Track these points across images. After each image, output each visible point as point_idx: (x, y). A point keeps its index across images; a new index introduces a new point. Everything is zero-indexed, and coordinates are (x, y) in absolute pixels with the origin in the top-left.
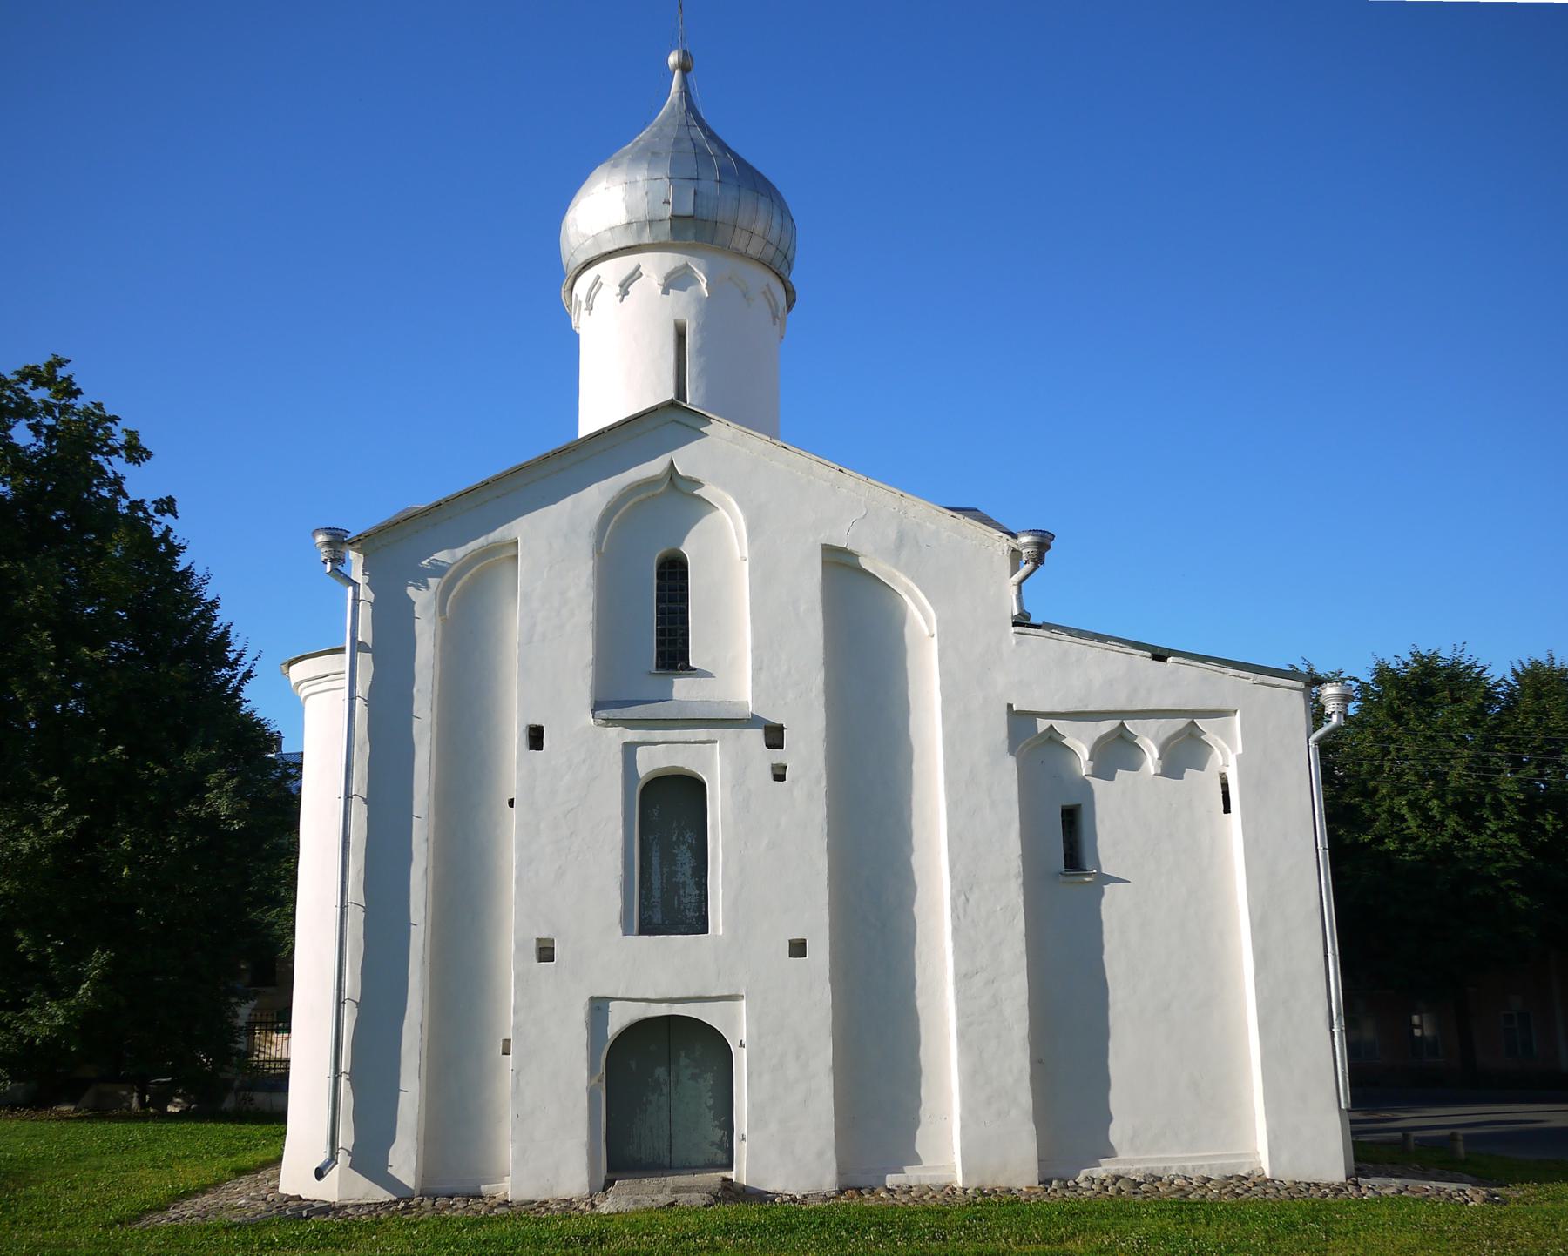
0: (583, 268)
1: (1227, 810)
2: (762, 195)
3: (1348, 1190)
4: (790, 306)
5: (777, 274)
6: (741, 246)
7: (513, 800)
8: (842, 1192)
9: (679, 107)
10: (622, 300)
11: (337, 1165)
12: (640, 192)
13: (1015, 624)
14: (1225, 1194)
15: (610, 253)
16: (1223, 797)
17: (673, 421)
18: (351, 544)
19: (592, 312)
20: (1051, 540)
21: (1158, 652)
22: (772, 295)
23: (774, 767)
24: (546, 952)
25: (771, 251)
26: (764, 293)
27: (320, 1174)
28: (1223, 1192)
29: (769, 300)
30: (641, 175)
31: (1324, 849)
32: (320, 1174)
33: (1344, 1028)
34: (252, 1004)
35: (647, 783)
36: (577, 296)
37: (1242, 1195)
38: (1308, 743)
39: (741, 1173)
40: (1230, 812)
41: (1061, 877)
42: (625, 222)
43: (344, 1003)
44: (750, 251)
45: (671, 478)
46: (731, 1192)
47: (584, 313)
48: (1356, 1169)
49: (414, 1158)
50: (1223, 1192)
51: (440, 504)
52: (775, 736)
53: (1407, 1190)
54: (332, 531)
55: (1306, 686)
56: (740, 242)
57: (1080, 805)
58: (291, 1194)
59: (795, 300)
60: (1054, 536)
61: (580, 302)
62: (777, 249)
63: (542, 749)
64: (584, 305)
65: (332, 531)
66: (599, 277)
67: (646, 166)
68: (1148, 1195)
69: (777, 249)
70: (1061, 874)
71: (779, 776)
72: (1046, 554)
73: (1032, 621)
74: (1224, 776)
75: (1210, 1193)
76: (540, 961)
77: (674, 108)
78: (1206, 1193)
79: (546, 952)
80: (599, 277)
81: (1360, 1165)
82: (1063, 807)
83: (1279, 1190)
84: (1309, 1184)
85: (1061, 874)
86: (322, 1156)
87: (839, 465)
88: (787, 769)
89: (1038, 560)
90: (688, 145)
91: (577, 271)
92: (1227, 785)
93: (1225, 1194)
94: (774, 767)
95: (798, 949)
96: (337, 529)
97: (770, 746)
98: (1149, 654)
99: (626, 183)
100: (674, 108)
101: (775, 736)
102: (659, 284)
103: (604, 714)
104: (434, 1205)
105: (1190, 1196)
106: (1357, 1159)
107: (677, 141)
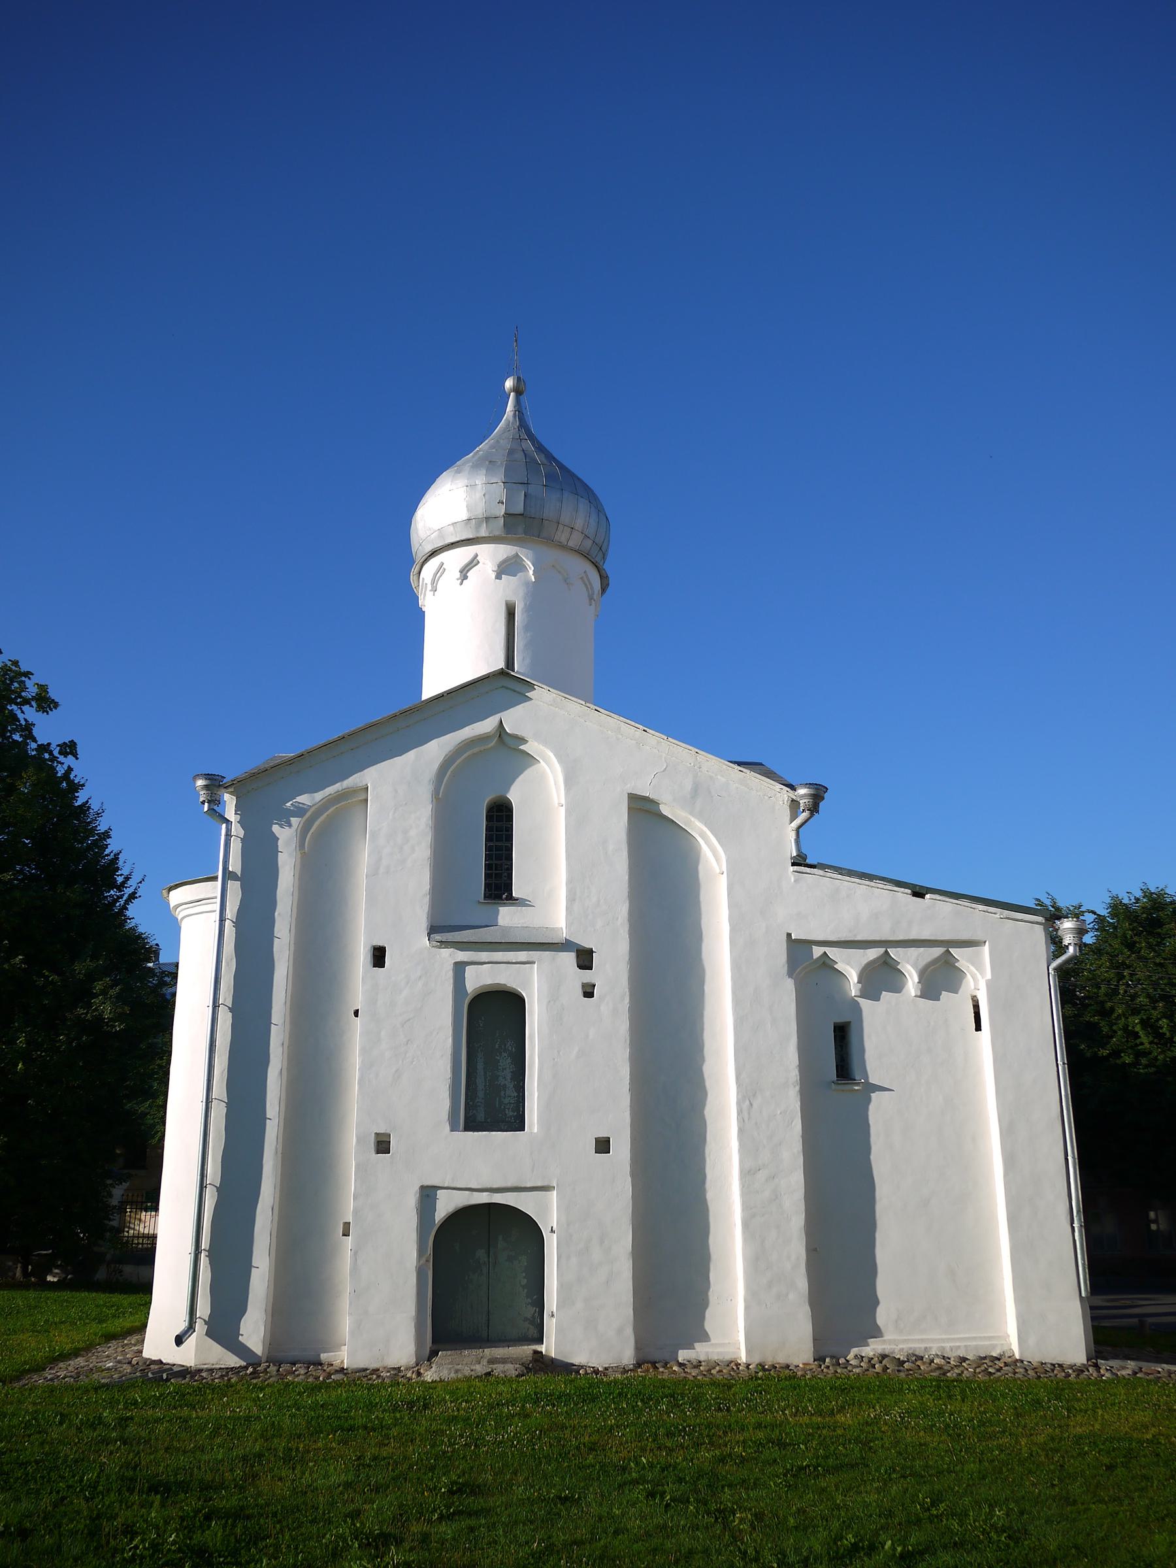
1: (978, 1028)
2: (582, 497)
3: (1088, 1371)
6: (563, 540)
7: (358, 1010)
12: (478, 494)
13: (793, 864)
14: (980, 1373)
18: (225, 788)
20: (825, 792)
21: (917, 889)
23: (584, 985)
24: (383, 1145)
25: (588, 543)
26: (582, 578)
27: (179, 1340)
28: (978, 1370)
29: (586, 585)
31: (1064, 1064)
32: (179, 1340)
36: (423, 581)
37: (994, 1373)
39: (550, 1347)
43: (206, 1187)
44: (571, 544)
46: (541, 1363)
47: (429, 594)
50: (978, 1370)
52: (585, 959)
57: (850, 1022)
58: (153, 1358)
59: (608, 585)
61: (426, 584)
63: (384, 967)
64: (429, 587)
74: (975, 999)
75: (965, 1372)
78: (962, 1372)
79: (383, 1145)
86: (182, 1325)
93: (980, 1373)
94: (584, 985)
95: (603, 1146)
97: (581, 967)
98: (909, 891)
99: (467, 486)
101: (585, 959)
103: (438, 937)
107: (511, 452)
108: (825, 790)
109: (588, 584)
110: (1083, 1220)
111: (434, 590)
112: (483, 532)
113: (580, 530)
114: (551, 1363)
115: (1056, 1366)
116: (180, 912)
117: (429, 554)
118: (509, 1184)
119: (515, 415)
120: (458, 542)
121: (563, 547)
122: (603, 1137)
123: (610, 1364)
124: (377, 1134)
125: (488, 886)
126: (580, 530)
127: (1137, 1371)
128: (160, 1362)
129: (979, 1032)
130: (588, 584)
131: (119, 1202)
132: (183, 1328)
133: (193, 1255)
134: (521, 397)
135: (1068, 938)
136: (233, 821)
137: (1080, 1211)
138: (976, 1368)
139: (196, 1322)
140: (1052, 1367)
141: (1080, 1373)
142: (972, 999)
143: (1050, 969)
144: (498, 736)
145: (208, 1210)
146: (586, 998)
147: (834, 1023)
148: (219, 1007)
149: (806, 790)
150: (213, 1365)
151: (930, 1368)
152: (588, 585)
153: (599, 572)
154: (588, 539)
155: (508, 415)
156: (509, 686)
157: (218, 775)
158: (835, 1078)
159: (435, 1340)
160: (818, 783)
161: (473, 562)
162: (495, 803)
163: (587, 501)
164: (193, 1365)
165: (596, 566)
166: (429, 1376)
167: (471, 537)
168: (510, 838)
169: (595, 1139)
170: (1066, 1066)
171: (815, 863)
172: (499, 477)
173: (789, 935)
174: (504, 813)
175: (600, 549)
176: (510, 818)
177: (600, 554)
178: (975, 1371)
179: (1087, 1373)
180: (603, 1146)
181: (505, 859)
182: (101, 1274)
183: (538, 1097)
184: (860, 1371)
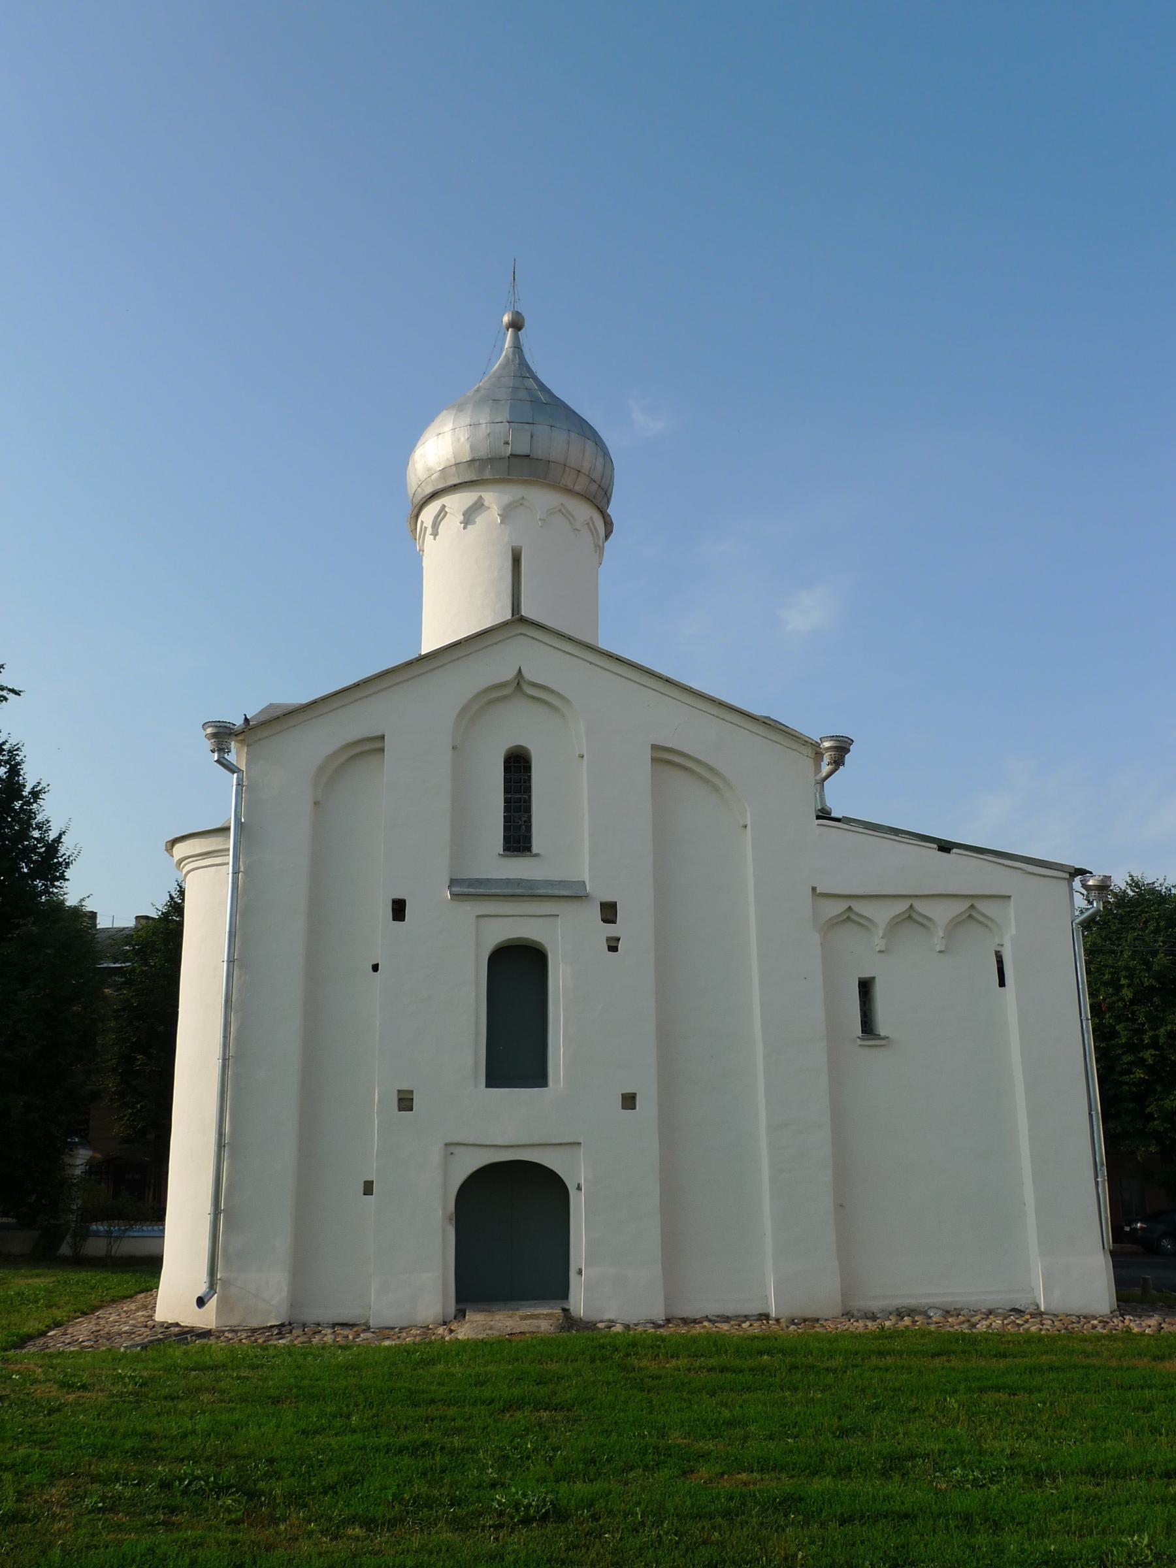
0: (430, 498)
1: (1002, 984)
2: (588, 439)
3: (1114, 1322)
4: (607, 537)
5: (599, 508)
6: (569, 484)
7: (377, 965)
8: (668, 1321)
9: (513, 361)
10: (465, 528)
11: (216, 1295)
12: (483, 430)
13: (818, 817)
14: (1008, 1324)
15: (455, 485)
16: (998, 968)
17: (521, 634)
18: (236, 735)
19: (437, 537)
20: (851, 744)
21: (943, 844)
22: (594, 526)
23: (609, 939)
24: (405, 1102)
25: (594, 487)
26: (588, 524)
27: (201, 1302)
28: (1005, 1322)
29: (591, 531)
30: (466, 420)
31: (1087, 1019)
32: (201, 1302)
33: (1106, 1178)
34: (35, 1195)
35: (502, 948)
36: (422, 522)
37: (1023, 1325)
38: (1072, 926)
39: (580, 1302)
40: (1004, 986)
41: (858, 1040)
42: (469, 459)
43: (224, 1146)
44: (577, 488)
45: (518, 684)
46: (569, 1322)
47: (429, 538)
48: (1118, 1306)
49: (286, 1289)
50: (1005, 1322)
51: (316, 702)
52: (609, 912)
53: (1165, 1322)
54: (216, 724)
55: (1070, 876)
56: (568, 480)
57: (873, 978)
58: (170, 1322)
59: (612, 532)
60: (852, 741)
61: (426, 528)
62: (600, 486)
63: (404, 920)
64: (429, 530)
65: (216, 724)
66: (444, 506)
67: (454, 412)
68: (941, 1325)
69: (600, 486)
70: (859, 1038)
71: (613, 948)
72: (846, 756)
73: (833, 815)
74: (999, 954)
75: (994, 1324)
76: (400, 1110)
77: (508, 362)
78: (991, 1324)
79: (405, 1102)
80: (444, 506)
81: (1119, 1303)
82: (859, 978)
83: (1053, 1322)
84: (1078, 1317)
85: (859, 1038)
86: (202, 1288)
87: (246, 769)
88: (620, 941)
89: (838, 762)
90: (523, 394)
91: (424, 500)
92: (1002, 961)
93: (1008, 1324)
94: (609, 939)
95: (629, 1101)
96: (225, 722)
97: (605, 921)
98: (935, 846)
99: (470, 425)
100: (508, 362)
101: (609, 912)
102: (499, 515)
103: (456, 889)
104: (304, 1331)
105: (978, 1326)
106: (1118, 1300)
107: (515, 389)
108: (849, 741)
109: (593, 529)
110: (1106, 1174)
111: (435, 534)
112: (487, 474)
113: (587, 473)
114: (579, 1320)
115: (1081, 1317)
116: (186, 864)
117: (429, 496)
118: (536, 1140)
119: (514, 353)
120: (461, 484)
121: (570, 491)
122: (629, 1093)
123: (639, 1321)
124: (399, 1091)
125: (506, 839)
126: (587, 473)
127: (1160, 1322)
128: (177, 1325)
129: (1003, 988)
130: (593, 529)
131: (82, 1172)
132: (204, 1289)
133: (212, 1215)
134: (519, 333)
135: (1093, 894)
136: (244, 770)
137: (1103, 1165)
138: (1003, 1320)
139: (217, 1283)
140: (1078, 1319)
141: (1105, 1324)
142: (996, 954)
143: (1074, 924)
144: (516, 683)
145: (226, 1170)
146: (611, 953)
147: (859, 978)
148: (234, 962)
149: (832, 742)
150: (235, 1327)
151: (958, 1321)
152: (593, 530)
153: (604, 517)
154: (594, 483)
155: (507, 352)
156: (528, 634)
157: (229, 723)
158: (860, 1034)
159: (459, 1299)
160: (844, 735)
161: (442, 513)
162: (512, 753)
163: (594, 443)
164: (214, 1327)
165: (601, 512)
166: (464, 1332)
167: (475, 479)
168: (528, 790)
169: (622, 1095)
170: (1090, 1021)
171: (840, 816)
172: (504, 415)
173: (814, 889)
174: (522, 764)
175: (606, 493)
176: (528, 769)
177: (606, 499)
178: (1003, 1323)
179: (1112, 1324)
180: (629, 1101)
181: (524, 812)
182: (65, 1249)
183: (563, 1051)
184: (890, 1324)
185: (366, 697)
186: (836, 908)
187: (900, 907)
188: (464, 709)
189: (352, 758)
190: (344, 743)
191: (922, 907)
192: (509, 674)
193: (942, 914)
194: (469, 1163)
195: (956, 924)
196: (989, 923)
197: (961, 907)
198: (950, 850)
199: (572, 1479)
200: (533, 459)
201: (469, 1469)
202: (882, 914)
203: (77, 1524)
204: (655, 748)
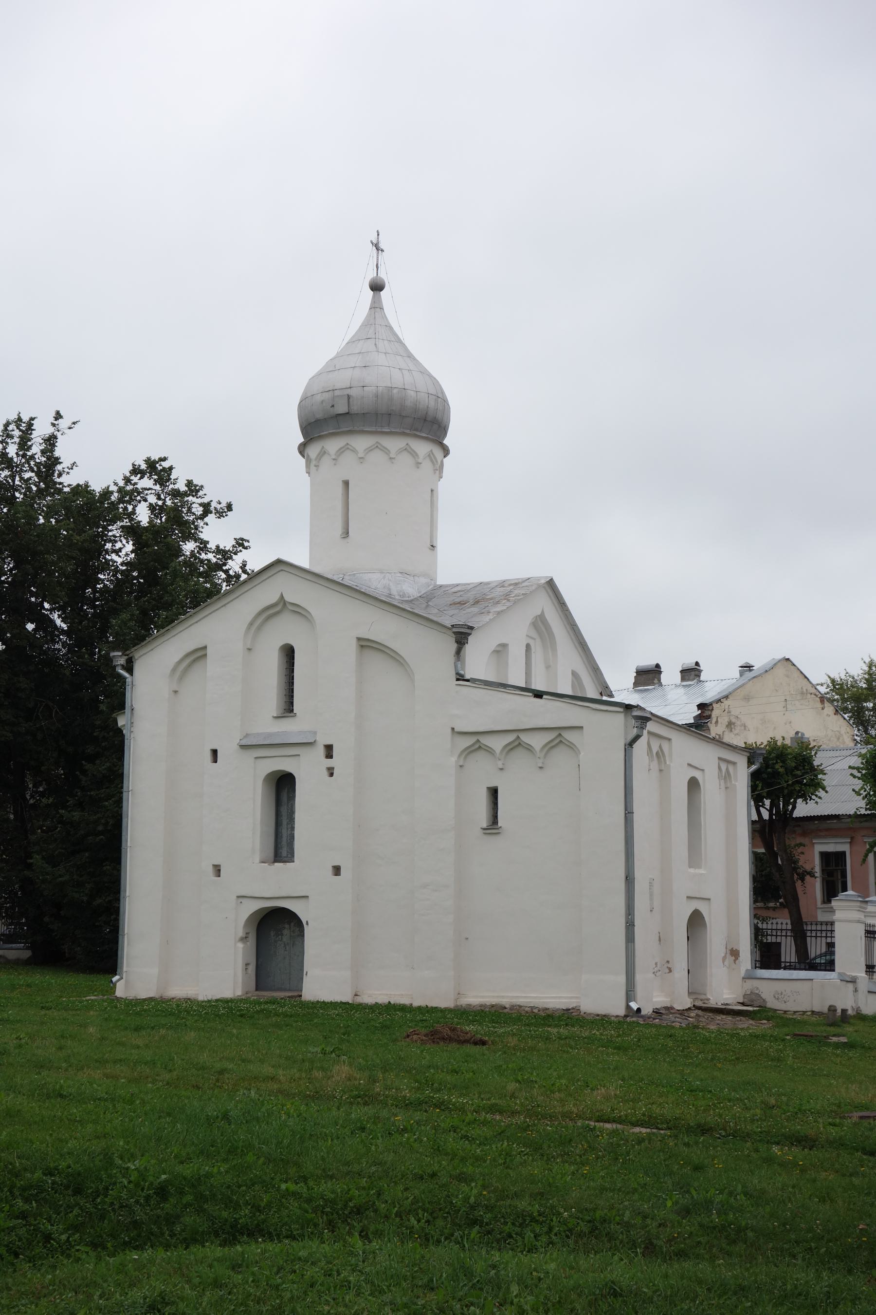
13: (458, 680)
17: (282, 570)
29: (411, 453)
52: (329, 751)
95: (337, 870)
98: (531, 694)
101: (329, 751)
173: (453, 729)
185: (196, 622)
186: (469, 741)
187: (511, 738)
188: (251, 624)
189: (194, 661)
190: (184, 653)
191: (525, 738)
192: (274, 598)
193: (537, 741)
194: (253, 907)
195: (550, 747)
196: (575, 749)
197: (550, 736)
198: (542, 696)
199: (729, 1230)
200: (351, 414)
201: (394, 1124)
202: (497, 744)
203: (202, 1152)
204: (359, 639)
